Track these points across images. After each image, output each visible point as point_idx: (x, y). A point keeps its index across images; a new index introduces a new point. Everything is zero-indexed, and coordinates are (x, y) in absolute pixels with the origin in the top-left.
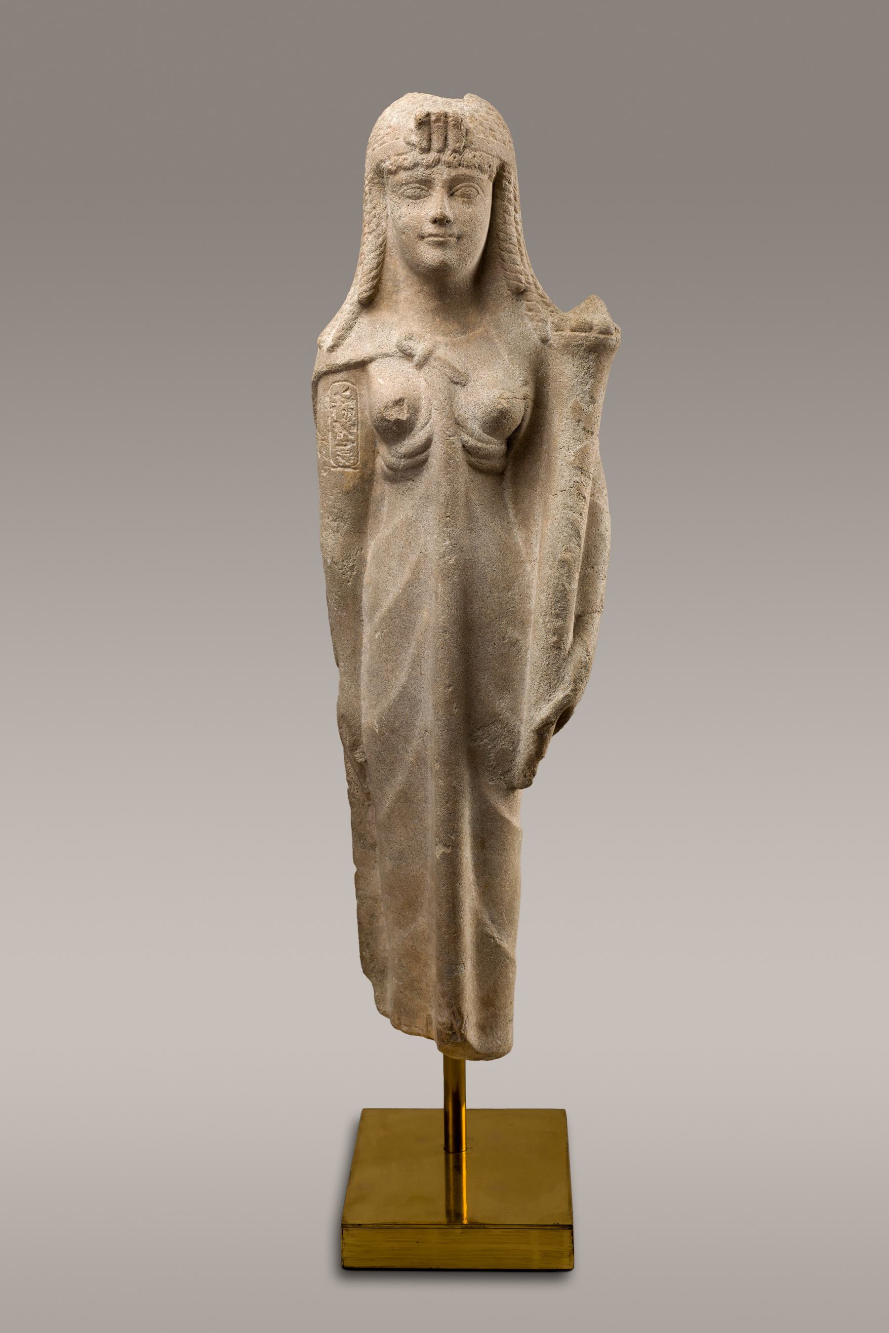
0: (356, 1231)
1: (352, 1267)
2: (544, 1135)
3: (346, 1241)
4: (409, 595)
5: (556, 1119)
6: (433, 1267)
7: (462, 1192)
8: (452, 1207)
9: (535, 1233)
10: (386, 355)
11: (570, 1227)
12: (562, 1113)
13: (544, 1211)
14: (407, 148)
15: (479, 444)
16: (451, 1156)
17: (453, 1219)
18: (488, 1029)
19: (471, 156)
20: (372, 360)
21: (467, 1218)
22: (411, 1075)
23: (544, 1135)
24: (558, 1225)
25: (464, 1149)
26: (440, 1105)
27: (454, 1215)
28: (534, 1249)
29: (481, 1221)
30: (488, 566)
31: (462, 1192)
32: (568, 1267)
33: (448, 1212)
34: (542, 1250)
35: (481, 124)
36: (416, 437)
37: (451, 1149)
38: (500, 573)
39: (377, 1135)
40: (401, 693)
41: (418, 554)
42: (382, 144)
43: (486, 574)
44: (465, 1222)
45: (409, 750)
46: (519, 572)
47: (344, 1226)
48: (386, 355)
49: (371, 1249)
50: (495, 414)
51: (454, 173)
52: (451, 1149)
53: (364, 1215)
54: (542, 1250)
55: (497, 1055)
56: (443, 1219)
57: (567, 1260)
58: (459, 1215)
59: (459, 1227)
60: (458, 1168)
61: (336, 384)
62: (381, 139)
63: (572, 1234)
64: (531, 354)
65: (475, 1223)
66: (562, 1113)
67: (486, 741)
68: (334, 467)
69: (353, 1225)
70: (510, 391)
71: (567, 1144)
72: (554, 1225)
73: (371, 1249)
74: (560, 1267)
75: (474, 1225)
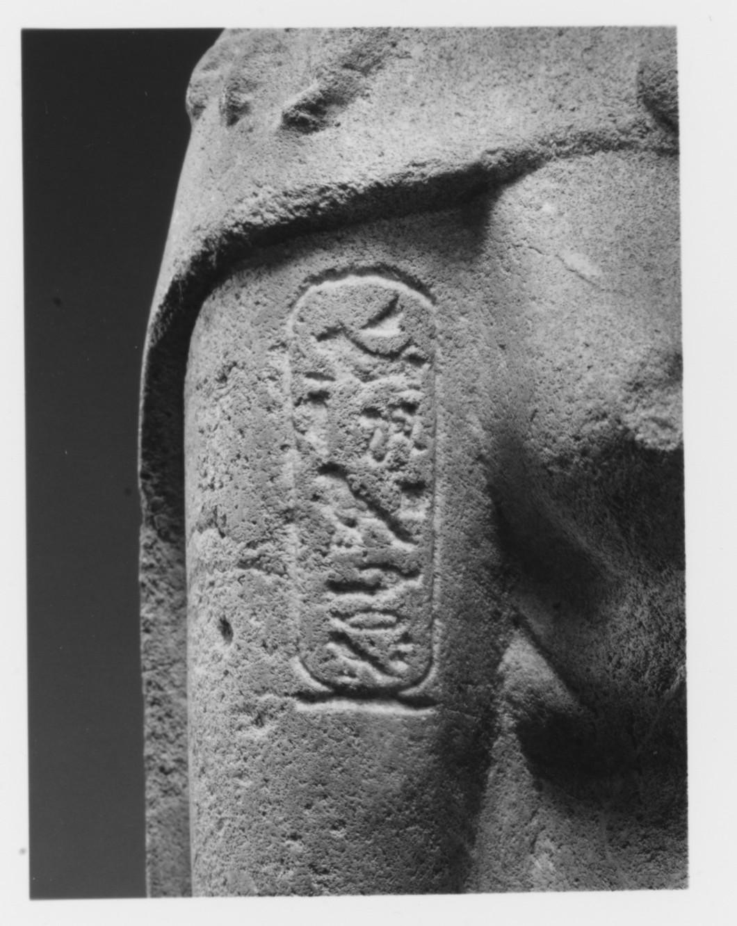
61: (328, 286)
68: (307, 696)
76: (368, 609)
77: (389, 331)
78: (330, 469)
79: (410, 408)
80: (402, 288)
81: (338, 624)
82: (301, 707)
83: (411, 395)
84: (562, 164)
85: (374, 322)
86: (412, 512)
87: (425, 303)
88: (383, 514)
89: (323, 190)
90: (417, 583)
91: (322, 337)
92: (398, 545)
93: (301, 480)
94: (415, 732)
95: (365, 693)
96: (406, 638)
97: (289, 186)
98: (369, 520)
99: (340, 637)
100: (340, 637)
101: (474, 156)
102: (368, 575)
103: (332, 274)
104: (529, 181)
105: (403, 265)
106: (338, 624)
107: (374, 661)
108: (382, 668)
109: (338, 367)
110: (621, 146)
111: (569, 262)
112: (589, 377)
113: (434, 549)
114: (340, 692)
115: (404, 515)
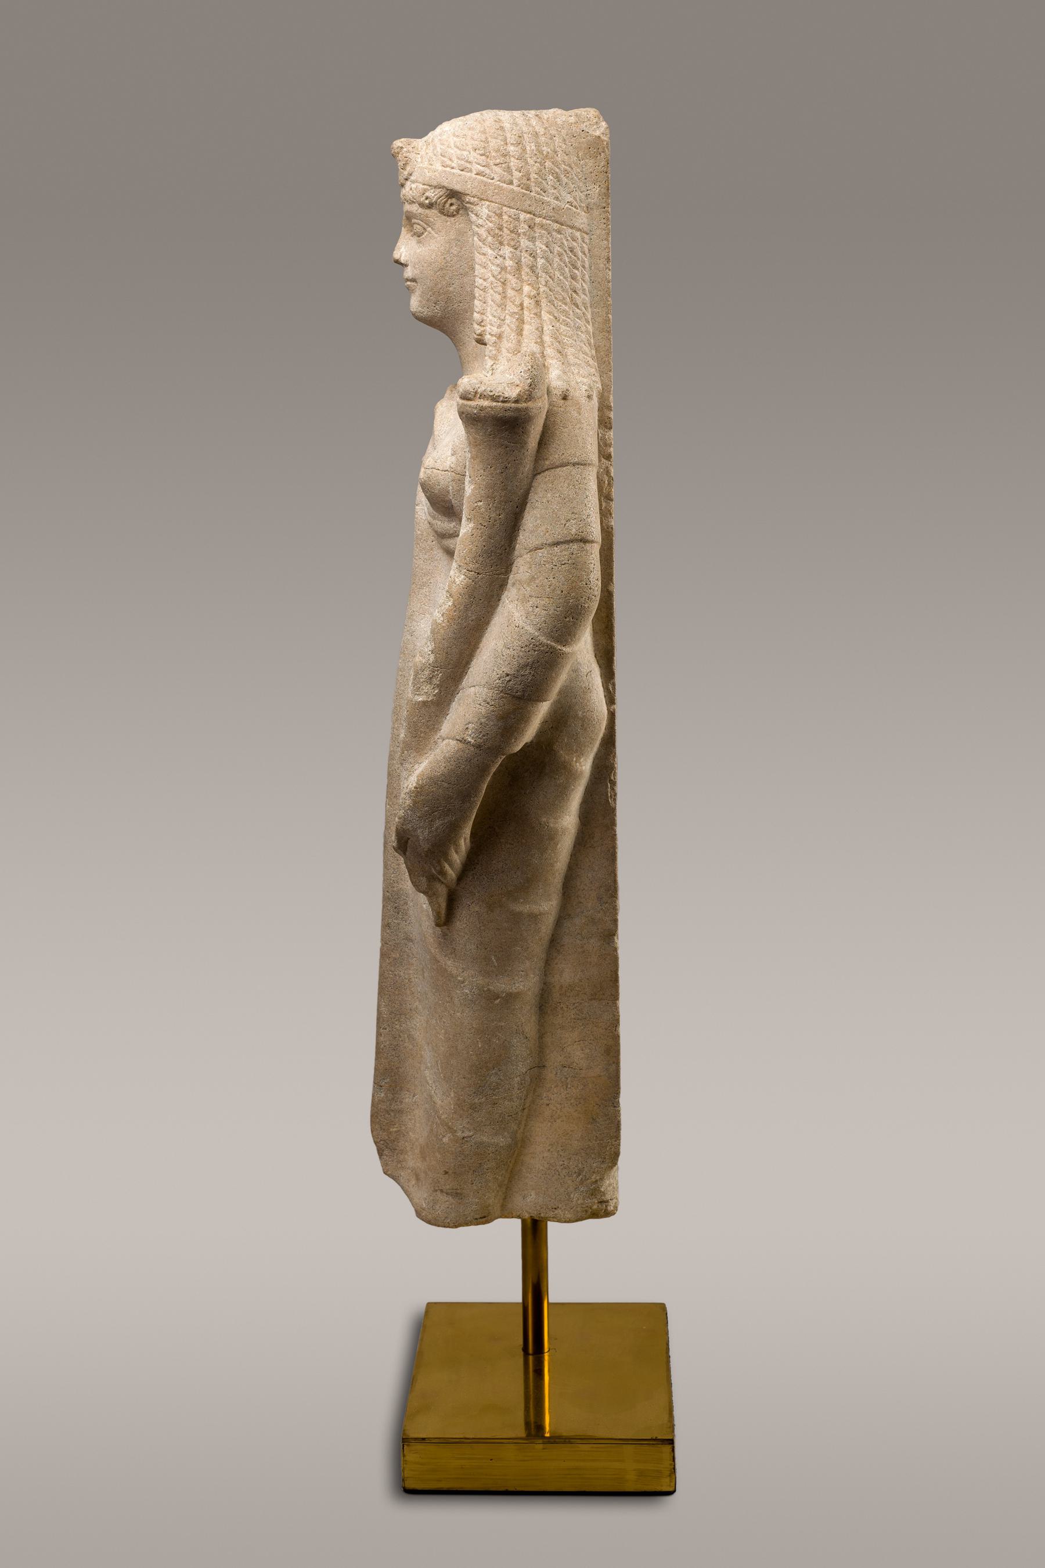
0: (420, 1447)
1: (411, 1489)
2: (641, 1332)
3: (407, 1458)
5: (654, 1317)
7: (542, 1404)
8: (532, 1419)
9: (629, 1449)
11: (671, 1442)
12: (662, 1308)
13: (640, 1422)
16: (531, 1358)
17: (533, 1432)
20: (436, 532)
21: (550, 1432)
22: (482, 1264)
23: (641, 1332)
24: (656, 1440)
25: (546, 1350)
26: (519, 1299)
27: (534, 1428)
28: (628, 1468)
29: (565, 1434)
31: (542, 1404)
32: (671, 1489)
33: (527, 1424)
34: (638, 1469)
37: (531, 1351)
39: (440, 1334)
44: (547, 1435)
47: (404, 1441)
49: (432, 1468)
52: (531, 1351)
53: (426, 1427)
54: (638, 1469)
55: (607, 1214)
56: (521, 1432)
57: (668, 1480)
58: (540, 1427)
59: (541, 1441)
60: (539, 1372)
63: (673, 1450)
65: (560, 1437)
66: (662, 1308)
69: (416, 1439)
71: (668, 1344)
72: (652, 1440)
73: (432, 1468)
74: (659, 1489)
75: (556, 1439)
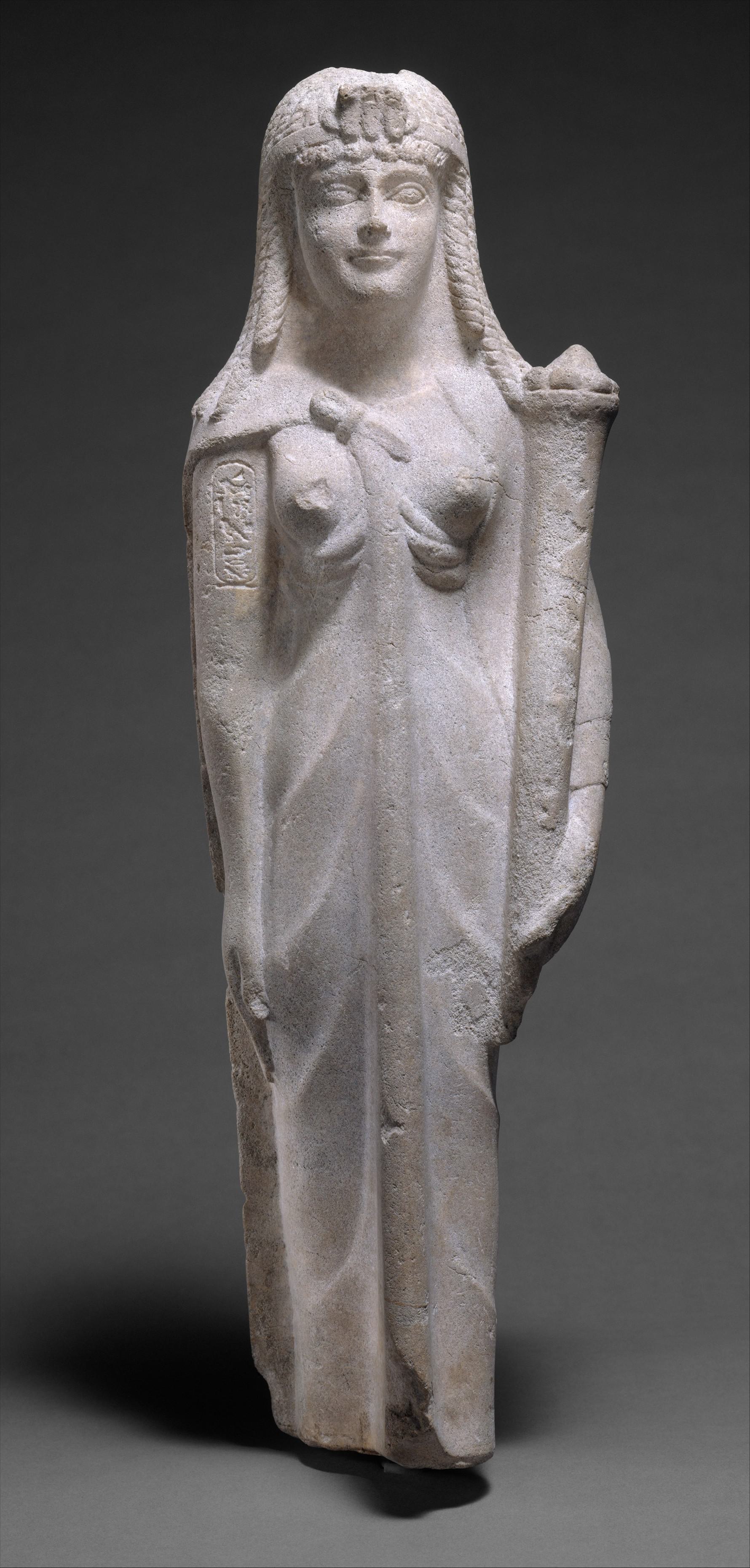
4: (334, 761)
6: (495, 1081)
10: (296, 423)
14: (321, 135)
15: (431, 543)
18: (461, 1418)
19: (414, 145)
30: (447, 717)
35: (425, 105)
36: (343, 533)
38: (464, 727)
40: (323, 905)
41: (347, 700)
42: (289, 133)
43: (443, 727)
45: (336, 990)
46: (490, 725)
48: (296, 423)
50: (452, 500)
51: (391, 167)
61: (224, 466)
62: (287, 127)
64: (497, 422)
67: (449, 971)
68: (220, 585)
70: (471, 468)
76: (235, 559)
77: (240, 479)
78: (224, 519)
79: (247, 501)
80: (245, 467)
81: (227, 564)
82: (217, 588)
83: (247, 497)
84: (288, 429)
85: (235, 477)
86: (247, 530)
87: (251, 470)
88: (240, 532)
89: (220, 438)
90: (250, 551)
91: (221, 482)
92: (244, 540)
93: (216, 523)
94: (251, 594)
95: (235, 583)
96: (247, 567)
97: (211, 437)
98: (236, 533)
99: (228, 567)
100: (228, 567)
101: (262, 428)
102: (235, 549)
103: (225, 463)
104: (278, 434)
105: (244, 459)
106: (227, 564)
107: (238, 574)
108: (240, 576)
109: (225, 490)
110: (305, 423)
111: (340, 453)
112: (288, 489)
113: (567, 788)
114: (229, 583)
115: (245, 532)
